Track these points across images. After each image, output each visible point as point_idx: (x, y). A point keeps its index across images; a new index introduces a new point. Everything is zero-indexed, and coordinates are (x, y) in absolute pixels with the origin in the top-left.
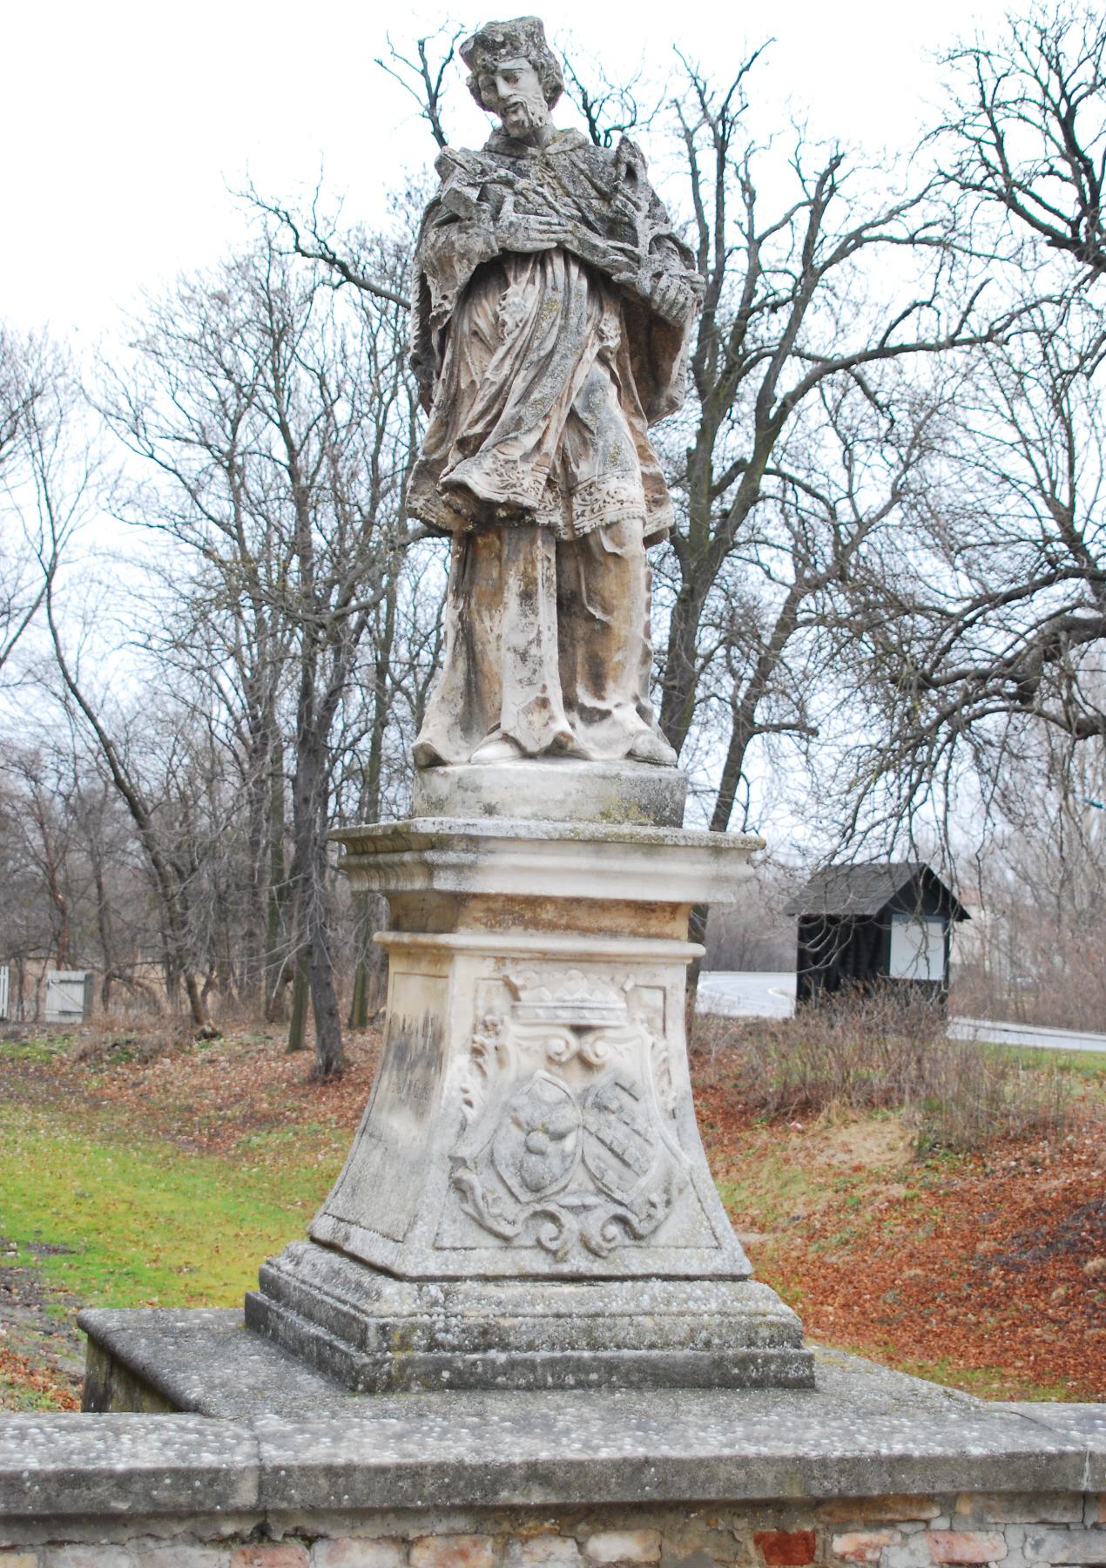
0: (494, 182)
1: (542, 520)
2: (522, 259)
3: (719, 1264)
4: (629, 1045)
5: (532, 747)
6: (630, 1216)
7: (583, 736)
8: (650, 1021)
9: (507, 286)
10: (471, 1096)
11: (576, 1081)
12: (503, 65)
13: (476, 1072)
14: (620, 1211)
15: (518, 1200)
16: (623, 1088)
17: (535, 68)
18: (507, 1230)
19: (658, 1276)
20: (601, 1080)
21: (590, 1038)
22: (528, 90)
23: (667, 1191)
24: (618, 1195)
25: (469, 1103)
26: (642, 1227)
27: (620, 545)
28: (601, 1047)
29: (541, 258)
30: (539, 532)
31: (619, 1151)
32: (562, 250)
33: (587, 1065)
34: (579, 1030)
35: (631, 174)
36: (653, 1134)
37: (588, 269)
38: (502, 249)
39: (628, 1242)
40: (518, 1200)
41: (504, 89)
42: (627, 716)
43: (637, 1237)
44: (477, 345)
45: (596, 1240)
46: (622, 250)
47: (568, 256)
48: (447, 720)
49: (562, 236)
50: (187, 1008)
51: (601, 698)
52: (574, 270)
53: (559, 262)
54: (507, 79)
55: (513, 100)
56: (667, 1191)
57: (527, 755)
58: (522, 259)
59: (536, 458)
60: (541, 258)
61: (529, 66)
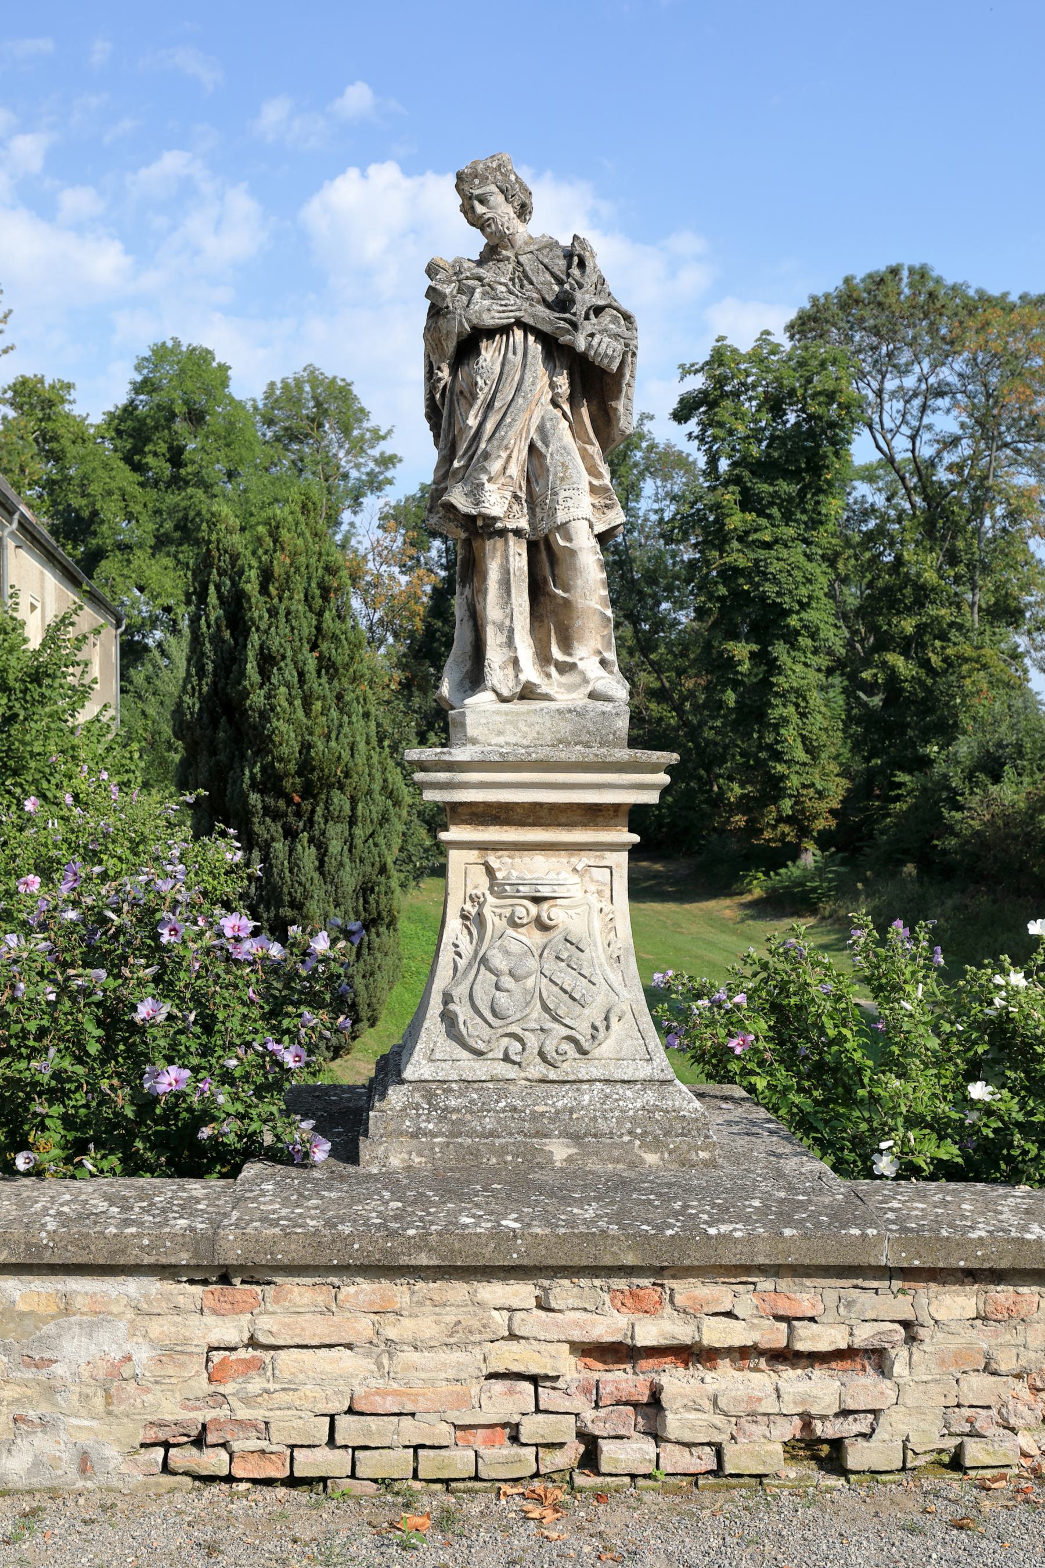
0: (467, 278)
1: (511, 525)
2: (490, 333)
3: (644, 1071)
4: (578, 910)
5: (506, 693)
6: (579, 1037)
7: (553, 684)
8: (599, 892)
9: (479, 354)
10: (462, 950)
11: (534, 938)
12: (476, 192)
13: (465, 931)
14: (570, 1032)
15: (490, 1026)
16: (572, 944)
17: (502, 191)
18: (481, 1046)
19: (600, 1081)
20: (556, 935)
21: (545, 905)
22: (503, 211)
23: (607, 1018)
24: (567, 1021)
25: (459, 955)
26: (586, 1045)
27: (570, 540)
28: (555, 913)
29: (505, 330)
30: (511, 535)
31: (569, 989)
32: (519, 323)
33: (543, 927)
34: (537, 900)
35: (582, 265)
36: (598, 979)
37: (542, 337)
38: (474, 328)
39: (577, 1056)
40: (490, 1026)
41: (480, 209)
42: (590, 666)
43: (585, 1053)
44: (462, 401)
45: (551, 1054)
46: (564, 320)
47: (527, 328)
48: (457, 676)
49: (518, 314)
50: (372, 898)
51: (570, 655)
52: (531, 338)
53: (519, 334)
54: (482, 202)
55: (486, 217)
56: (607, 1018)
57: (503, 700)
58: (490, 333)
59: (502, 480)
60: (505, 330)
61: (497, 190)
